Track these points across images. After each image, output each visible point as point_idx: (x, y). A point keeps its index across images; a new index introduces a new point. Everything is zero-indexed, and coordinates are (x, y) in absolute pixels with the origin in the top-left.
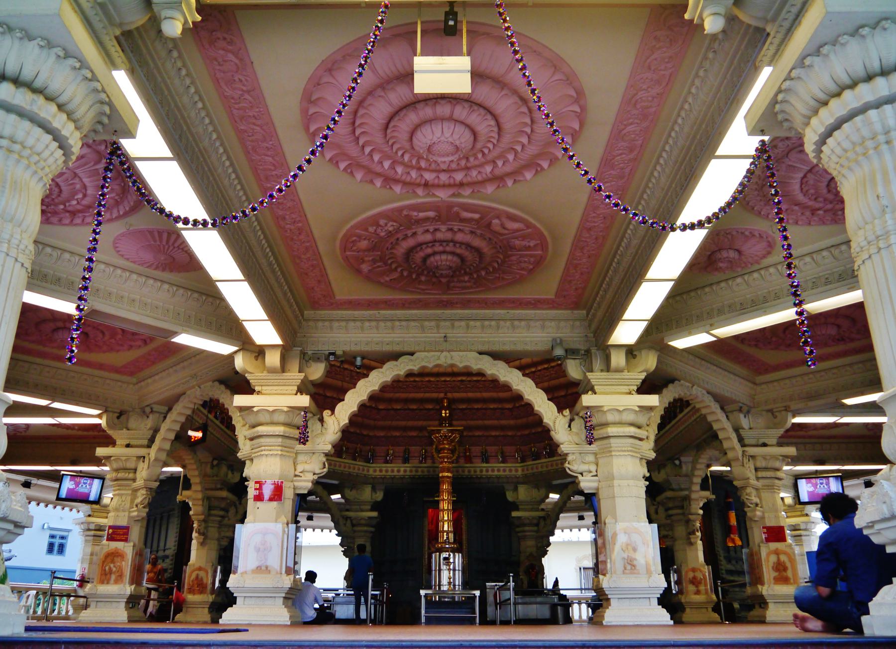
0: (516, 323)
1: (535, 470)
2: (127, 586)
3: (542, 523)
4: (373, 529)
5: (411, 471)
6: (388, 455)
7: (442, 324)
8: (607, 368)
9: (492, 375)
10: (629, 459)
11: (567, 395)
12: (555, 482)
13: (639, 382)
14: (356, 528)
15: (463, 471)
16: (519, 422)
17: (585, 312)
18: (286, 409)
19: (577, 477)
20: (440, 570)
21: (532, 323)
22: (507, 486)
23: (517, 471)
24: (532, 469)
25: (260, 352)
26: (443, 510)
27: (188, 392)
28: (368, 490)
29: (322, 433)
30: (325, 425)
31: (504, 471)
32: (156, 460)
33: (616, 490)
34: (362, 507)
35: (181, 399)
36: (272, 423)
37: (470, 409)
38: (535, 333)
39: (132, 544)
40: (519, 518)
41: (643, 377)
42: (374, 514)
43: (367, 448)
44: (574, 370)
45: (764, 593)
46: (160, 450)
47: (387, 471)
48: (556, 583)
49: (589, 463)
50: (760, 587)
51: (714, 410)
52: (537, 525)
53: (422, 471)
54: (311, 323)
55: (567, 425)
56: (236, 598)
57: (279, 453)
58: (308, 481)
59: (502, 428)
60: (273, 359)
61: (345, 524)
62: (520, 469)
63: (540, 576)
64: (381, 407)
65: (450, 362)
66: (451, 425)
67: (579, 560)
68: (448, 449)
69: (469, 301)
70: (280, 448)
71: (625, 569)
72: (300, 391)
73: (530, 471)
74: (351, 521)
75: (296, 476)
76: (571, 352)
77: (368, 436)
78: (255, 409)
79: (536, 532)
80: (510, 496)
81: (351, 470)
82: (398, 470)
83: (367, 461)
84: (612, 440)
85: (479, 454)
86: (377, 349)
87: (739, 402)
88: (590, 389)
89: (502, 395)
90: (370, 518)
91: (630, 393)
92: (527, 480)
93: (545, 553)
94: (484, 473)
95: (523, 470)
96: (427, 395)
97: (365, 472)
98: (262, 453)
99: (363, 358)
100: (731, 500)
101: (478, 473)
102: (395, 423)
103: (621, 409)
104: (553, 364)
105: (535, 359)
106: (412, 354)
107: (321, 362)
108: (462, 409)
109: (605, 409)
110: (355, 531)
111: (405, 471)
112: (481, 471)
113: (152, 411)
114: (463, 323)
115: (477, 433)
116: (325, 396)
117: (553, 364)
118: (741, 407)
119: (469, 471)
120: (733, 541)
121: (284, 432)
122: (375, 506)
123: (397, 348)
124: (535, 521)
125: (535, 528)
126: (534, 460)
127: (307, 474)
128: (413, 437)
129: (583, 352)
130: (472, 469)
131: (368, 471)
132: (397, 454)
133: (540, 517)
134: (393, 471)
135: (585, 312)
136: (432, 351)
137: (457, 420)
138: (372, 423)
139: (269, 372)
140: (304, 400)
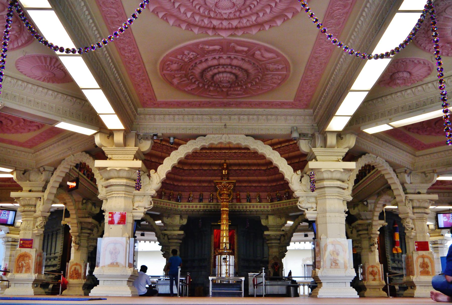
0: (269, 117)
1: (279, 207)
3: (282, 238)
4: (181, 241)
5: (204, 207)
6: (190, 197)
7: (224, 117)
10: (336, 201)
11: (299, 162)
12: (291, 214)
13: (344, 154)
15: (235, 207)
16: (270, 178)
17: (312, 110)
18: (127, 169)
19: (304, 211)
20: (221, 265)
21: (279, 117)
22: (262, 217)
23: (268, 207)
25: (110, 134)
26: (223, 230)
27: (66, 159)
28: (177, 218)
29: (149, 184)
32: (48, 199)
34: (174, 228)
37: (240, 170)
39: (35, 250)
41: (347, 151)
42: (182, 232)
44: (304, 146)
46: (50, 193)
47: (189, 207)
48: (290, 273)
49: (311, 203)
50: (411, 277)
52: (280, 239)
53: (211, 207)
55: (299, 180)
56: (99, 281)
57: (124, 195)
59: (259, 181)
60: (119, 138)
61: (164, 238)
62: (270, 206)
63: (280, 269)
66: (228, 179)
67: (304, 260)
68: (227, 194)
69: (241, 103)
70: (124, 192)
71: (332, 265)
72: (136, 157)
73: (276, 208)
75: (134, 209)
76: (303, 135)
78: (108, 169)
79: (279, 243)
80: (263, 222)
81: (167, 206)
82: (196, 206)
83: (177, 201)
84: (326, 189)
85: (245, 197)
87: (405, 167)
88: (314, 158)
90: (179, 235)
91: (338, 161)
93: (284, 256)
94: (248, 208)
95: (272, 207)
96: (214, 161)
97: (176, 208)
100: (397, 226)
101: (244, 208)
102: (194, 178)
105: (281, 140)
106: (205, 136)
107: (149, 140)
109: (323, 170)
110: (170, 243)
111: (200, 207)
112: (246, 207)
113: (44, 170)
114: (236, 117)
116: (151, 161)
117: (291, 143)
118: (406, 170)
119: (239, 207)
121: (126, 183)
122: (182, 228)
124: (278, 237)
125: (279, 241)
126: (278, 201)
127: (140, 208)
129: (310, 135)
130: (241, 206)
131: (178, 207)
132: (195, 197)
133: (281, 235)
134: (193, 207)
136: (217, 134)
137: (231, 176)
138: (180, 178)
140: (139, 164)
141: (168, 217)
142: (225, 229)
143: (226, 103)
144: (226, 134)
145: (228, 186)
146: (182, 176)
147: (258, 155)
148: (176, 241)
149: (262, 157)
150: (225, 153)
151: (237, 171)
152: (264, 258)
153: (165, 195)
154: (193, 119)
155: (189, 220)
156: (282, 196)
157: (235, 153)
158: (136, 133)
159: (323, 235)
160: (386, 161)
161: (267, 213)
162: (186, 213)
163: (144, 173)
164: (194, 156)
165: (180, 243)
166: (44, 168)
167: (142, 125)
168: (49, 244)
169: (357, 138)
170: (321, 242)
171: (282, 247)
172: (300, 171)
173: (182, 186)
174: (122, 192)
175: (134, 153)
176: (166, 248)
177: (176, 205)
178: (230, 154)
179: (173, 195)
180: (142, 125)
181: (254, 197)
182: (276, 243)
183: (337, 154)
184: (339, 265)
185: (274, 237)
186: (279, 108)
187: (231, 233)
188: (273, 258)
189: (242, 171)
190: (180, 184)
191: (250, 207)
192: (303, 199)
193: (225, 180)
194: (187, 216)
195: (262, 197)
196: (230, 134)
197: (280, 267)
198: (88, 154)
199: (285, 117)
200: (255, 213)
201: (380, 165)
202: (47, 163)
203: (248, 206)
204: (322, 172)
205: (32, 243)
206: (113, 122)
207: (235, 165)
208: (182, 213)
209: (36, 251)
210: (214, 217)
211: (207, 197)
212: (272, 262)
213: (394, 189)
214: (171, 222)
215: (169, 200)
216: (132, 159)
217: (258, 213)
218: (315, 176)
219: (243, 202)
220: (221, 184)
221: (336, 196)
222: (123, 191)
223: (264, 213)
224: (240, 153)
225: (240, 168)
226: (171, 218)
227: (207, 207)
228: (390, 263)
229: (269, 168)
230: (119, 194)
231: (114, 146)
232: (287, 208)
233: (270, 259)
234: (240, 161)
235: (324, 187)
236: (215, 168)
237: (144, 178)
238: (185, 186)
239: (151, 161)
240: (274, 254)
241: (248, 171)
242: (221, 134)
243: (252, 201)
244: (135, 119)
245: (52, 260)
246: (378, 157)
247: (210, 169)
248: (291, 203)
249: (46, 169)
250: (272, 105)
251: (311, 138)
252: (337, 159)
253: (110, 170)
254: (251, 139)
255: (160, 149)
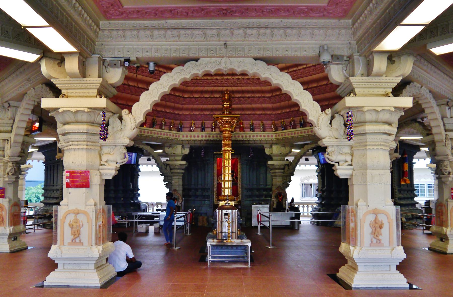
0: (289, 31)
1: (284, 136)
2: (7, 227)
3: (287, 168)
4: (183, 171)
5: (206, 136)
6: (191, 126)
7: (223, 32)
8: (369, 72)
9: (255, 74)
10: (381, 152)
11: (329, 95)
12: (295, 143)
13: (394, 85)
14: (172, 171)
15: (239, 136)
16: (275, 105)
17: (350, 21)
18: (86, 110)
19: (334, 165)
20: (222, 222)
21: (303, 32)
22: (265, 146)
23: (272, 136)
24: (282, 135)
25: (60, 58)
26: (225, 159)
27: (28, 92)
28: (179, 147)
29: (121, 130)
30: (123, 121)
31: (264, 136)
32: (15, 142)
33: (369, 178)
34: (177, 158)
35: (25, 97)
36: (77, 122)
37: (243, 97)
38: (304, 40)
39: (8, 200)
40: (273, 165)
41: (399, 81)
42: (184, 163)
43: (178, 122)
44: (336, 74)
45: (448, 233)
46: (16, 135)
47: (191, 137)
48: (293, 200)
49: (345, 154)
50: (445, 229)
51: (433, 105)
52: (284, 169)
53: (213, 137)
54: (106, 33)
55: (329, 122)
56: (57, 264)
57: (85, 147)
58: (112, 169)
59: (264, 109)
60: (72, 65)
61: (166, 169)
62: (274, 135)
63: (284, 199)
64: (186, 96)
65: (229, 67)
66: (230, 113)
67: (302, 180)
68: (229, 131)
69: (247, 9)
70: (85, 143)
71: (372, 242)
72: (100, 94)
73: (281, 137)
74: (170, 167)
75: (101, 165)
76: (336, 58)
77: (178, 114)
78: (60, 111)
79: (283, 173)
80: (267, 151)
81: (168, 136)
82: (199, 136)
83: (179, 130)
84: (368, 137)
85: (249, 126)
86: (166, 55)
87: (448, 98)
88: (351, 91)
89: (264, 88)
90: (181, 165)
91: (387, 95)
92: (278, 142)
93: (287, 186)
94: (252, 137)
95: (276, 136)
96: (216, 88)
97: (177, 137)
98: (71, 147)
99: (156, 65)
100: (406, 156)
101: (248, 138)
102: (195, 106)
103: (379, 109)
104: (300, 68)
105: (288, 64)
106: (197, 60)
107: (118, 67)
108: (239, 98)
109: (365, 109)
110: (172, 173)
111: (202, 136)
112: (250, 136)
113: (9, 106)
114: (241, 32)
115: (248, 113)
116: (123, 97)
117: (300, 68)
118: (448, 102)
119: (242, 137)
120: (405, 181)
121: (87, 129)
122: (185, 158)
123: (183, 55)
124: (282, 167)
125: (282, 171)
126: (283, 130)
127: (111, 163)
128: (207, 115)
129: (345, 58)
130: (244, 135)
131: (179, 136)
132: (197, 126)
133: (286, 165)
134: (194, 136)
135: (350, 21)
136: (214, 57)
137: (234, 104)
138: (180, 106)
139: (71, 77)
140: (102, 102)
141: (169, 147)
142: (227, 165)
143: (226, 10)
144: (226, 57)
145: (230, 122)
146: (182, 104)
147: (299, 110)
148: (178, 171)
149: (267, 84)
150: (227, 79)
151: (240, 99)
152: (267, 185)
153: (165, 125)
154: (179, 36)
155: (191, 149)
156: (287, 124)
157: (238, 79)
158: (99, 58)
159: (361, 200)
160: (430, 92)
161: (271, 142)
162: (187, 142)
163: (114, 114)
164: (194, 83)
165: (182, 173)
166: (9, 104)
167: (108, 45)
168: (52, 175)
169: (415, 61)
170: (359, 212)
171: (286, 177)
172: (330, 109)
173: (183, 115)
174: (82, 143)
175: (98, 87)
176: (169, 178)
177: (177, 135)
178: (232, 81)
179: (174, 124)
180: (108, 45)
181: (258, 126)
182: (280, 173)
183: (384, 85)
184: (382, 242)
185: (278, 167)
186: (303, 18)
187: (234, 161)
188: (277, 188)
189: (246, 99)
190: (181, 113)
191: (254, 136)
192: (333, 149)
193: (227, 114)
194: (189, 146)
195: (266, 126)
196: (232, 57)
197: (282, 195)
198: (48, 88)
199: (311, 31)
200: (259, 142)
201: (424, 97)
202: (9, 97)
203: (252, 135)
204: (364, 112)
205: (3, 193)
206: (55, 41)
207: (238, 92)
208: (184, 142)
209: (10, 201)
210: (215, 146)
211: (209, 126)
212: (275, 192)
213: (433, 126)
214: (173, 152)
215: (170, 130)
216: (96, 95)
217: (262, 142)
218: (353, 118)
219: (247, 131)
220: (221, 120)
221: (380, 145)
222: (84, 141)
223: (268, 142)
224: (243, 79)
225: (243, 96)
226: (173, 148)
227: (209, 137)
228: (396, 194)
229: (274, 95)
230: (79, 145)
231: (68, 77)
232: (292, 138)
233: (274, 188)
234: (244, 88)
235: (365, 134)
236: (217, 96)
237: (113, 122)
238: (186, 115)
239: (123, 97)
240: (277, 183)
241: (252, 98)
242: (220, 57)
243: (256, 130)
244: (97, 36)
245: (55, 192)
246: (423, 87)
247: (212, 96)
248: (297, 132)
249: (11, 105)
250: (294, 12)
251: (347, 62)
252: (383, 93)
253: (62, 112)
254: (262, 64)
255: (156, 76)
